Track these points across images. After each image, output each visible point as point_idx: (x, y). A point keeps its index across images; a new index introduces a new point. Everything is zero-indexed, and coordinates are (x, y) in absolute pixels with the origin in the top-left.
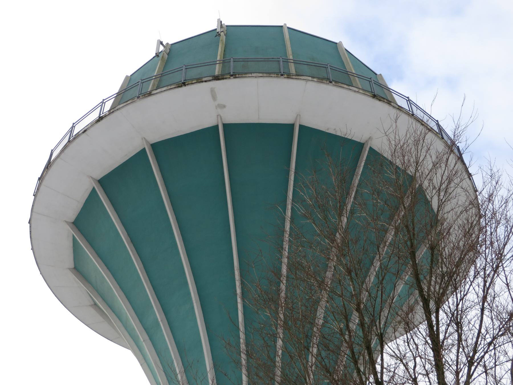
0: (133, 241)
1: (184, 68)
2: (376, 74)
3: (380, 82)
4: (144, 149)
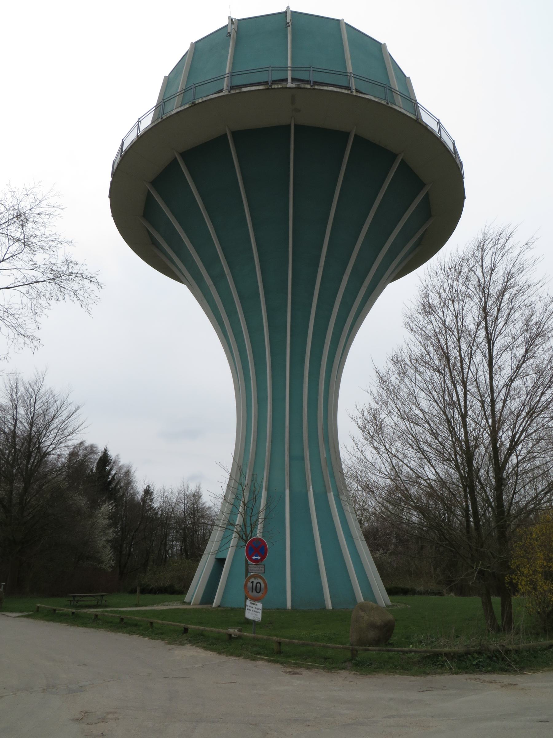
0: (207, 208)
1: (193, 87)
2: (405, 76)
3: (411, 97)
4: (176, 158)
